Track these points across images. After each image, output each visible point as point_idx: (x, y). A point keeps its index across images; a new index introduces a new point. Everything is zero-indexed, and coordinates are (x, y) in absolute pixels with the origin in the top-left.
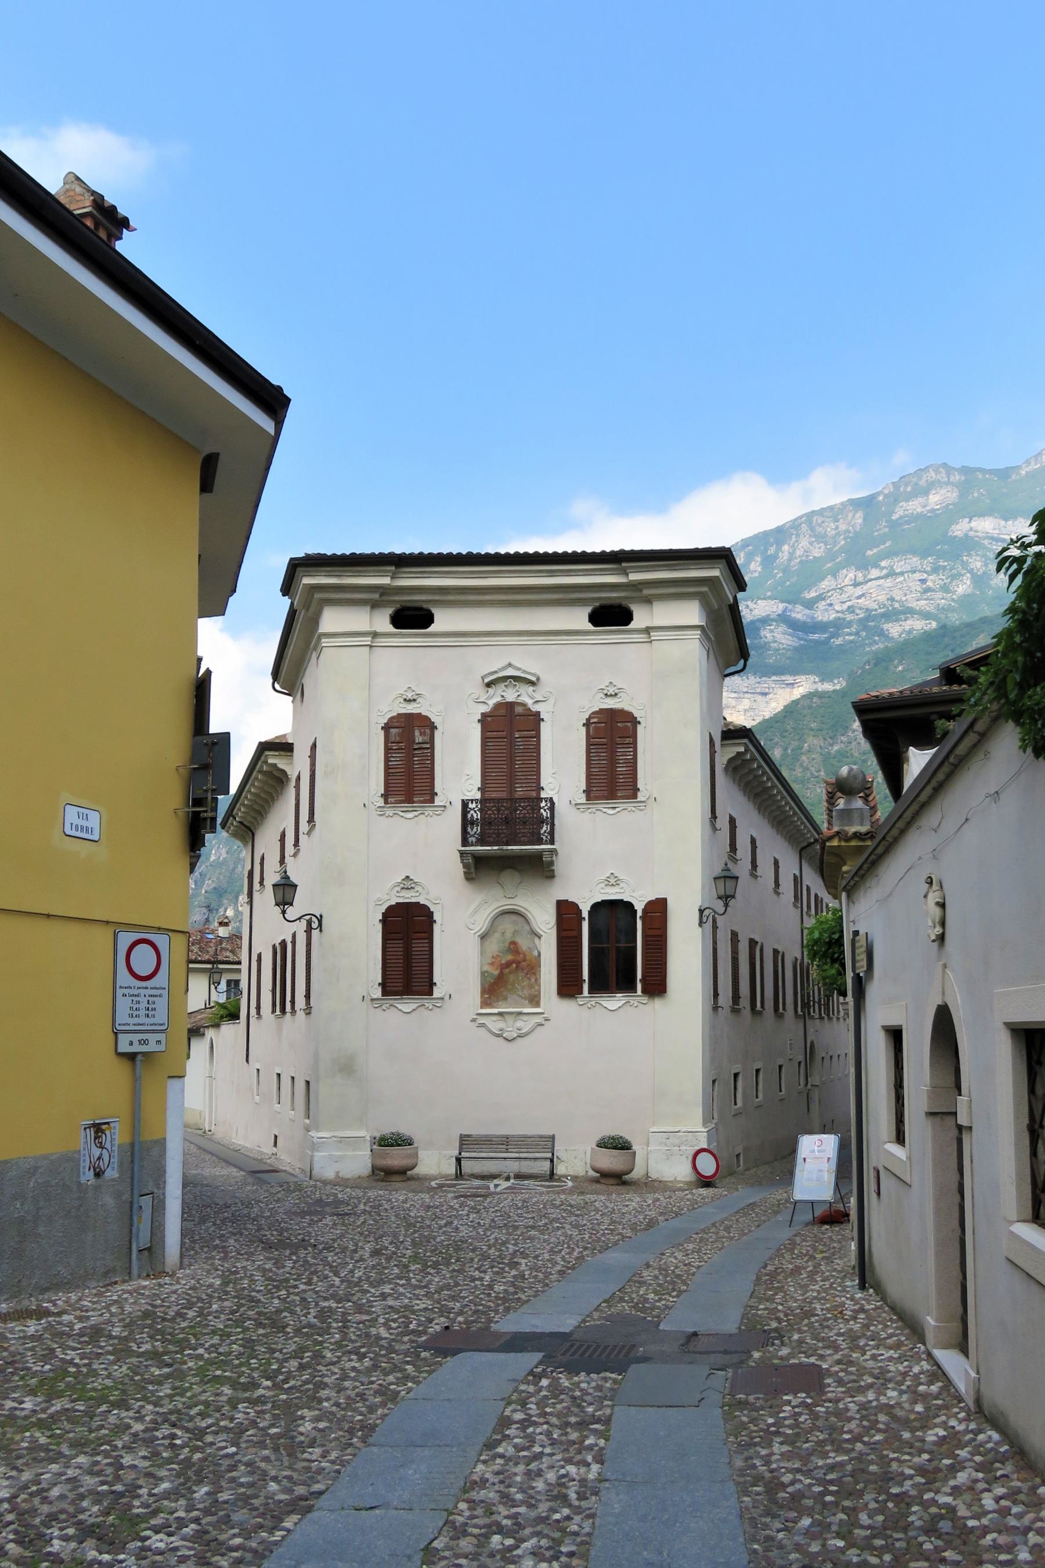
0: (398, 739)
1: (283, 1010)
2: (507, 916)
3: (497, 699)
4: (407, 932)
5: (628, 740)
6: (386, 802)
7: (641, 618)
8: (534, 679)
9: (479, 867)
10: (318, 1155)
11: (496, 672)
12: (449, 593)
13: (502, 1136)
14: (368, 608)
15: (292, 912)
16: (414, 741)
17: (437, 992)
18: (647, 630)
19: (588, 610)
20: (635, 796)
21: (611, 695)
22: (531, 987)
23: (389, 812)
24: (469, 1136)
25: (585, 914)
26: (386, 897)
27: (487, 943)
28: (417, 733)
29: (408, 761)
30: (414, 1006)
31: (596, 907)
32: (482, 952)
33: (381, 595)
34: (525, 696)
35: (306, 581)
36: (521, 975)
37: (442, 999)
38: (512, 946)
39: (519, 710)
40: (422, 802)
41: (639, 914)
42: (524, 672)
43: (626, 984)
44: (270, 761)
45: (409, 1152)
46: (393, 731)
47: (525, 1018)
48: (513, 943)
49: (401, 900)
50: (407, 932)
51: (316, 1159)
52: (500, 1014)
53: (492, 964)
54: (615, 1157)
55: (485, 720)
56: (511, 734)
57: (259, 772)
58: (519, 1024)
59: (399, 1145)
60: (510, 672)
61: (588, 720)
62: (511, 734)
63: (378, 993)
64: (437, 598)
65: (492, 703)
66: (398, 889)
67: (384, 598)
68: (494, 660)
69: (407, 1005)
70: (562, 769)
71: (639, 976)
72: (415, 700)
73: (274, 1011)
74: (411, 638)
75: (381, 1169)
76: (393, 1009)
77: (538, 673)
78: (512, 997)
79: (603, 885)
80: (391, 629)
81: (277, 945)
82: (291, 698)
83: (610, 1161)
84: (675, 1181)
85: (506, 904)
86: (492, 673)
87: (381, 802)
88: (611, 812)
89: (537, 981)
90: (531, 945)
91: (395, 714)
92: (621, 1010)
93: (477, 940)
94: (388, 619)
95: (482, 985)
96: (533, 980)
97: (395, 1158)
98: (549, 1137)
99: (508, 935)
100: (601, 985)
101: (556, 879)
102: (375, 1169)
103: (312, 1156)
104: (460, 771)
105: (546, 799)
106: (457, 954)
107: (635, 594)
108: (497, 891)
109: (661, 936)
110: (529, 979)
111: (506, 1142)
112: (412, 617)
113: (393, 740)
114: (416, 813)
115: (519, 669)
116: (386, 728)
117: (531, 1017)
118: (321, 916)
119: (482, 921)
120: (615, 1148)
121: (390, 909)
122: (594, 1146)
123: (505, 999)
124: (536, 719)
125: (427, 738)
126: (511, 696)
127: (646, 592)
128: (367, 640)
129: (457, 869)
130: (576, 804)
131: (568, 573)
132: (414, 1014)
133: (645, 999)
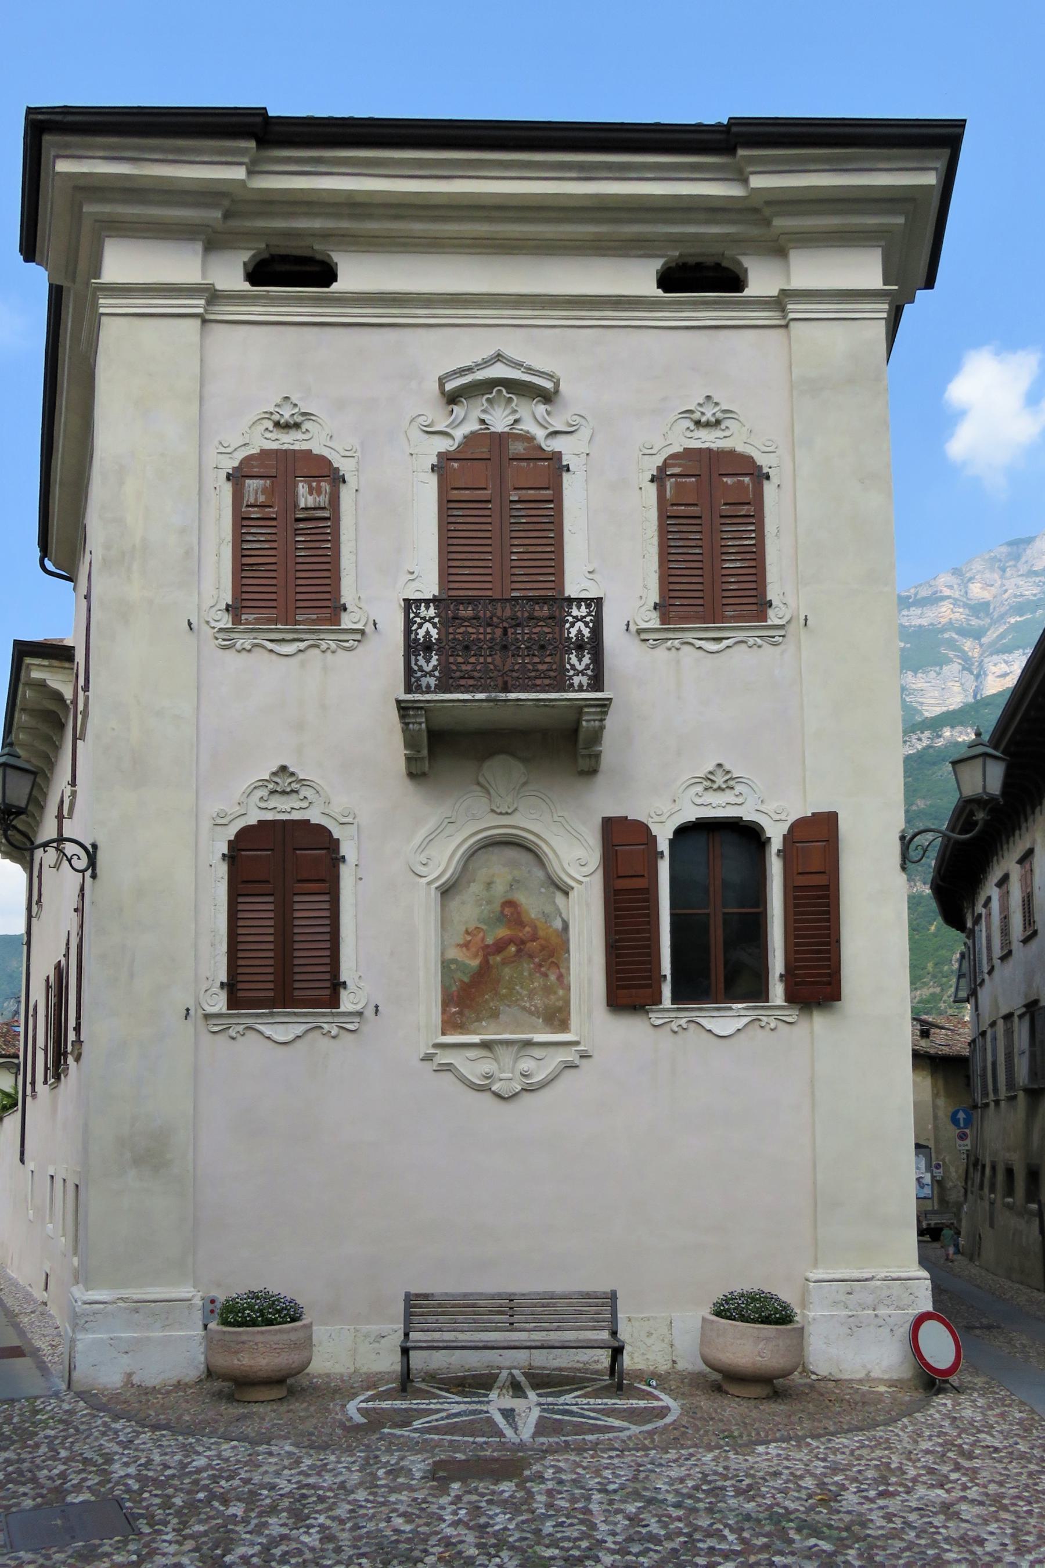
0: (262, 499)
2: (496, 850)
3: (472, 426)
4: (282, 892)
5: (744, 510)
6: (237, 620)
7: (762, 280)
8: (548, 385)
9: (440, 748)
10: (85, 1339)
11: (469, 370)
12: (370, 217)
13: (499, 1296)
14: (199, 247)
16: (296, 505)
17: (348, 1002)
18: (780, 302)
20: (334, 1002)
21: (708, 425)
22: (548, 990)
23: (244, 641)
24: (426, 1296)
25: (663, 846)
26: (237, 810)
27: (454, 904)
28: (302, 489)
29: (284, 555)
30: (300, 1029)
31: (683, 832)
32: (444, 923)
33: (227, 215)
34: (531, 420)
35: (63, 166)
36: (527, 967)
37: (360, 1014)
38: (507, 911)
39: (517, 448)
40: (313, 622)
41: (776, 844)
42: (530, 370)
43: (744, 984)
44: (35, 674)
45: (293, 1336)
46: (252, 484)
47: (538, 1052)
48: (510, 904)
49: (269, 816)
50: (282, 892)
51: (79, 1346)
52: (486, 1045)
53: (466, 945)
54: (767, 1339)
55: (443, 466)
56: (500, 497)
58: (526, 1064)
59: (270, 1323)
61: (662, 469)
62: (500, 497)
63: (219, 1003)
64: (344, 224)
65: (459, 434)
66: (264, 793)
67: (234, 224)
68: (464, 349)
69: (283, 1027)
70: (609, 552)
71: (777, 964)
72: (297, 426)
75: (225, 1377)
76: (251, 1035)
77: (559, 373)
78: (507, 1013)
79: (699, 789)
80: (247, 286)
83: (747, 1347)
84: (868, 1379)
85: (493, 825)
87: (226, 621)
89: (562, 980)
90: (548, 909)
91: (256, 451)
92: (742, 1035)
93: (434, 895)
94: (240, 273)
95: (445, 989)
96: (553, 978)
97: (261, 1351)
98: (604, 1296)
99: (500, 889)
100: (695, 986)
101: (600, 779)
102: (210, 1373)
103: (73, 1341)
104: (393, 554)
105: (589, 602)
106: (392, 922)
107: (754, 231)
108: (477, 802)
109: (827, 887)
110: (546, 975)
111: (509, 1308)
112: (292, 268)
113: (252, 501)
114: (302, 645)
115: (517, 365)
116: (237, 477)
117: (551, 1050)
118: (95, 846)
119: (443, 859)
120: (766, 1320)
121: (245, 833)
122: (706, 1311)
123: (495, 1015)
124: (555, 467)
125: (323, 500)
126: (500, 421)
127: (781, 223)
128: (197, 305)
129: (389, 747)
130: (639, 631)
131: (621, 173)
132: (299, 1044)
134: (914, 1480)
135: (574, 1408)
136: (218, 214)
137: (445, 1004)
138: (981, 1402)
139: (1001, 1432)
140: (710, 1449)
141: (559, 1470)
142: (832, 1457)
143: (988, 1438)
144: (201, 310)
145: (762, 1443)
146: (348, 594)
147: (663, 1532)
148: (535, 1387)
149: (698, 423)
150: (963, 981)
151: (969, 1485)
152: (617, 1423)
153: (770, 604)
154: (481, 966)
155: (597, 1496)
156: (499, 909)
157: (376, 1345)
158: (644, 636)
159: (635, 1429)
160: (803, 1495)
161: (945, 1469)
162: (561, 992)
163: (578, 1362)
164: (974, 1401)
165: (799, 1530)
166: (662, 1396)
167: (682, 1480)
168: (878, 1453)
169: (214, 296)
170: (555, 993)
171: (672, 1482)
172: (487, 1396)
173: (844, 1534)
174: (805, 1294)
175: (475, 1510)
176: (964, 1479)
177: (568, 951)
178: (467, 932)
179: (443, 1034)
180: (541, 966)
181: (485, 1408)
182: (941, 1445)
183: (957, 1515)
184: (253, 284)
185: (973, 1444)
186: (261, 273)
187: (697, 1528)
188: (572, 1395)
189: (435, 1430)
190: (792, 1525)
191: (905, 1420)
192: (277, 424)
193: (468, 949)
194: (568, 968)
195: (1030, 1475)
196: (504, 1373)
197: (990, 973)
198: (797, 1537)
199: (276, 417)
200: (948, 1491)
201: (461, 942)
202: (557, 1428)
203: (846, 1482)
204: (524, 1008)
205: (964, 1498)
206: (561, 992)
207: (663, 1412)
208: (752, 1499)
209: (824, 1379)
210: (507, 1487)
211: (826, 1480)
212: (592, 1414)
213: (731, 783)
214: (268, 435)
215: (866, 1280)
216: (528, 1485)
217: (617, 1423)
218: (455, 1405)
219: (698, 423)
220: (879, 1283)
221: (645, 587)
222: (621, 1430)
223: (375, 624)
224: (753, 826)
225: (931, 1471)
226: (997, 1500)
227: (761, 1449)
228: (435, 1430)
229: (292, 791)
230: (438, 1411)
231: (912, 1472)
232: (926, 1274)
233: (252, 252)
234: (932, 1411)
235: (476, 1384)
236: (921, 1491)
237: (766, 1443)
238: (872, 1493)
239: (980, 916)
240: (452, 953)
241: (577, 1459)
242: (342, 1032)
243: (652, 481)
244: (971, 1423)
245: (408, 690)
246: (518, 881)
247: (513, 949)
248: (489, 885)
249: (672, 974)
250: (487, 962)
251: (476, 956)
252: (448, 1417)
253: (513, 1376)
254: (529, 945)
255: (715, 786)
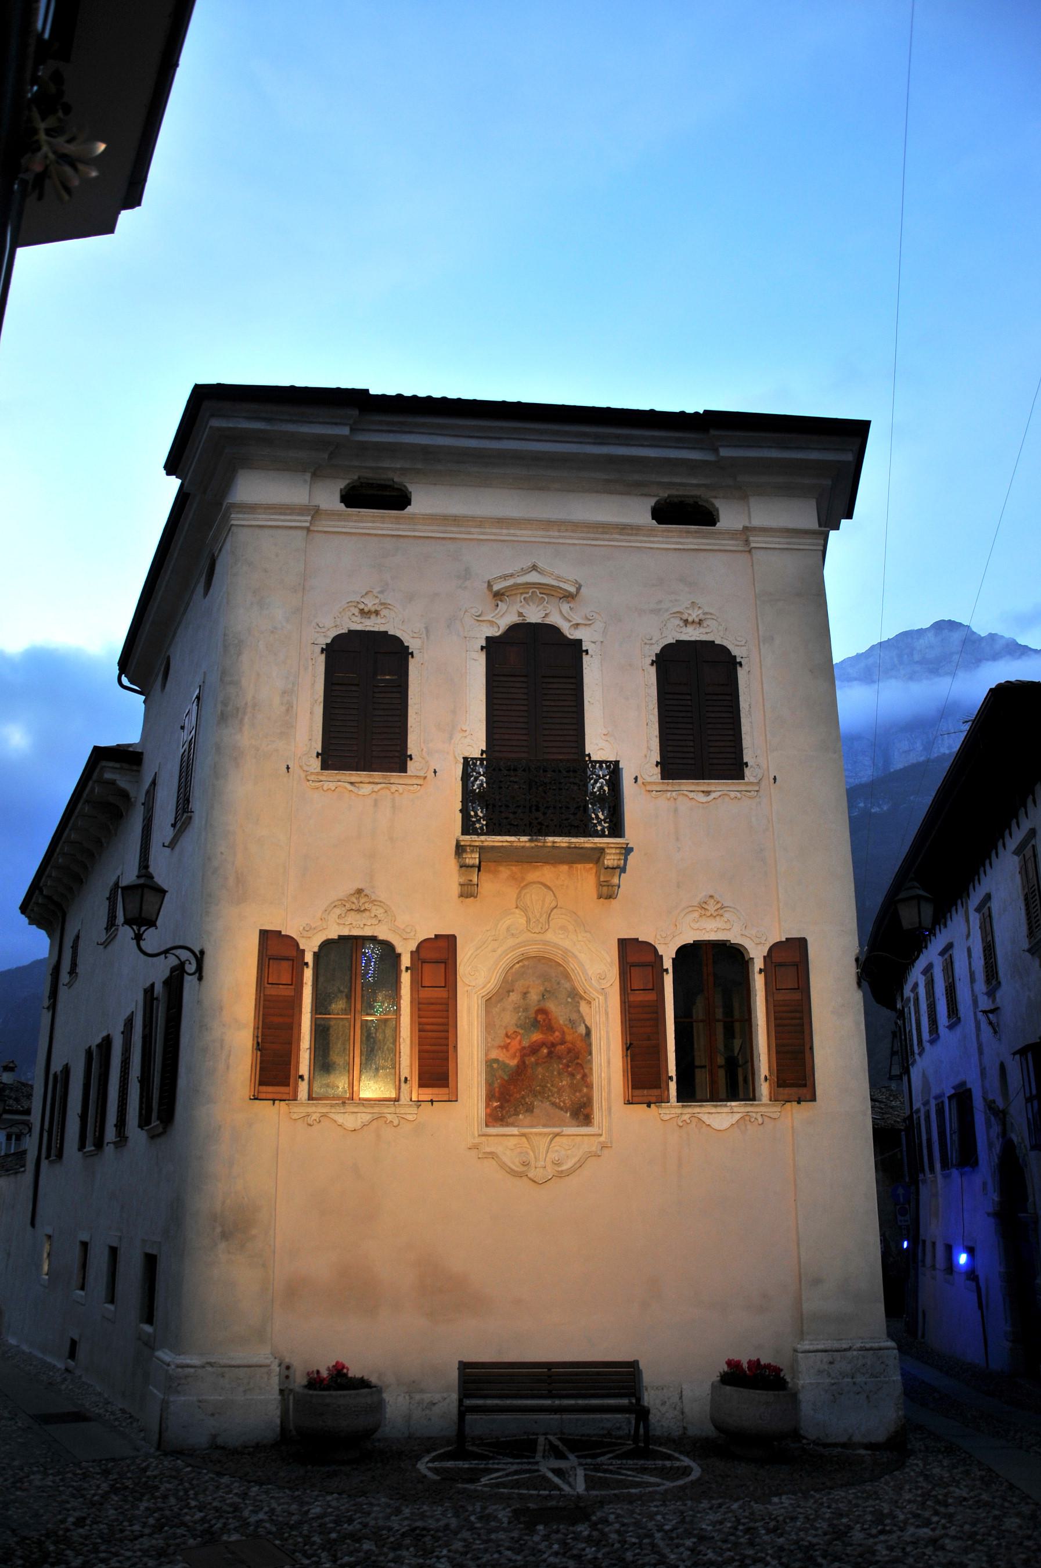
1: (99, 1144)
8: (572, 589)
14: (308, 476)
15: (152, 940)
19: (652, 502)
25: (668, 964)
35: (216, 423)
36: (557, 1066)
38: (540, 1017)
41: (758, 964)
43: (736, 1085)
44: (108, 776)
48: (542, 1011)
53: (506, 1047)
55: (493, 647)
56: (535, 673)
57: (87, 801)
60: (533, 577)
62: (535, 673)
70: (619, 723)
72: (377, 613)
73: (82, 1146)
74: (373, 521)
81: (94, 1048)
82: (143, 698)
83: (751, 1409)
86: (505, 577)
88: (702, 798)
89: (586, 1081)
91: (345, 631)
94: (337, 497)
95: (489, 1084)
96: (578, 1077)
104: (450, 719)
110: (572, 1075)
118: (202, 952)
126: (534, 615)
128: (305, 521)
133: (774, 1110)
134: (905, 1522)
135: (611, 1467)
136: (326, 456)
137: (490, 1097)
138: (945, 1463)
139: (966, 1486)
140: (737, 1500)
141: (618, 1516)
142: (834, 1506)
143: (957, 1490)
144: (308, 524)
145: (776, 1496)
146: (412, 748)
147: (720, 1559)
148: (572, 1451)
149: (686, 622)
150: (896, 1058)
151: (948, 1525)
152: (652, 1480)
153: (746, 764)
154: (518, 1066)
155: (658, 1535)
156: (533, 1015)
157: (428, 1412)
158: (649, 788)
159: (669, 1485)
160: (820, 1532)
161: (927, 1514)
162: (585, 1090)
163: (603, 1428)
164: (941, 1461)
165: (824, 1557)
166: (682, 1458)
167: (721, 1523)
168: (871, 1502)
169: (316, 513)
170: (580, 1091)
171: (713, 1524)
172: (534, 1457)
173: (860, 1560)
174: (795, 1361)
175: (564, 1543)
176: (943, 1521)
177: (590, 1053)
178: (507, 1036)
179: (487, 1126)
180: (568, 1066)
181: (536, 1467)
182: (920, 1496)
183: (943, 1548)
184: (347, 506)
185: (946, 1495)
186: (353, 498)
187: (745, 1557)
188: (607, 1457)
189: (503, 1485)
190: (818, 1553)
191: (887, 1477)
192: (362, 611)
193: (508, 1050)
194: (591, 1069)
195: (995, 1518)
196: (541, 1439)
197: (920, 1054)
198: (824, 1562)
199: (362, 606)
200: (933, 1530)
201: (502, 1044)
202: (604, 1484)
203: (851, 1524)
204: (554, 1104)
205: (947, 1535)
206: (585, 1090)
207: (686, 1471)
208: (781, 1535)
209: (816, 1443)
210: (583, 1529)
211: (835, 1522)
212: (629, 1473)
213: (721, 912)
214: (354, 619)
215: (845, 1350)
216: (599, 1526)
217: (652, 1480)
218: (508, 1467)
219: (686, 622)
220: (855, 1353)
221: (648, 748)
222: (659, 1485)
223: (435, 772)
224: (739, 950)
225: (916, 1516)
226: (972, 1536)
227: (776, 1500)
228: (503, 1485)
229: (365, 910)
230: (497, 1470)
231: (902, 1517)
232: (891, 1344)
233: (347, 482)
234: (907, 1470)
235: (521, 1448)
236: (911, 1530)
237: (779, 1495)
238: (874, 1531)
239: (909, 999)
240: (494, 1054)
241: (630, 1507)
242: (402, 1121)
243: (652, 664)
244: (941, 1478)
245: (465, 831)
246: (549, 992)
247: (545, 1051)
248: (525, 994)
249: (677, 1075)
250: (524, 1062)
251: (514, 1056)
252: (507, 1475)
253: (550, 1443)
254: (559, 1047)
255: (709, 914)
